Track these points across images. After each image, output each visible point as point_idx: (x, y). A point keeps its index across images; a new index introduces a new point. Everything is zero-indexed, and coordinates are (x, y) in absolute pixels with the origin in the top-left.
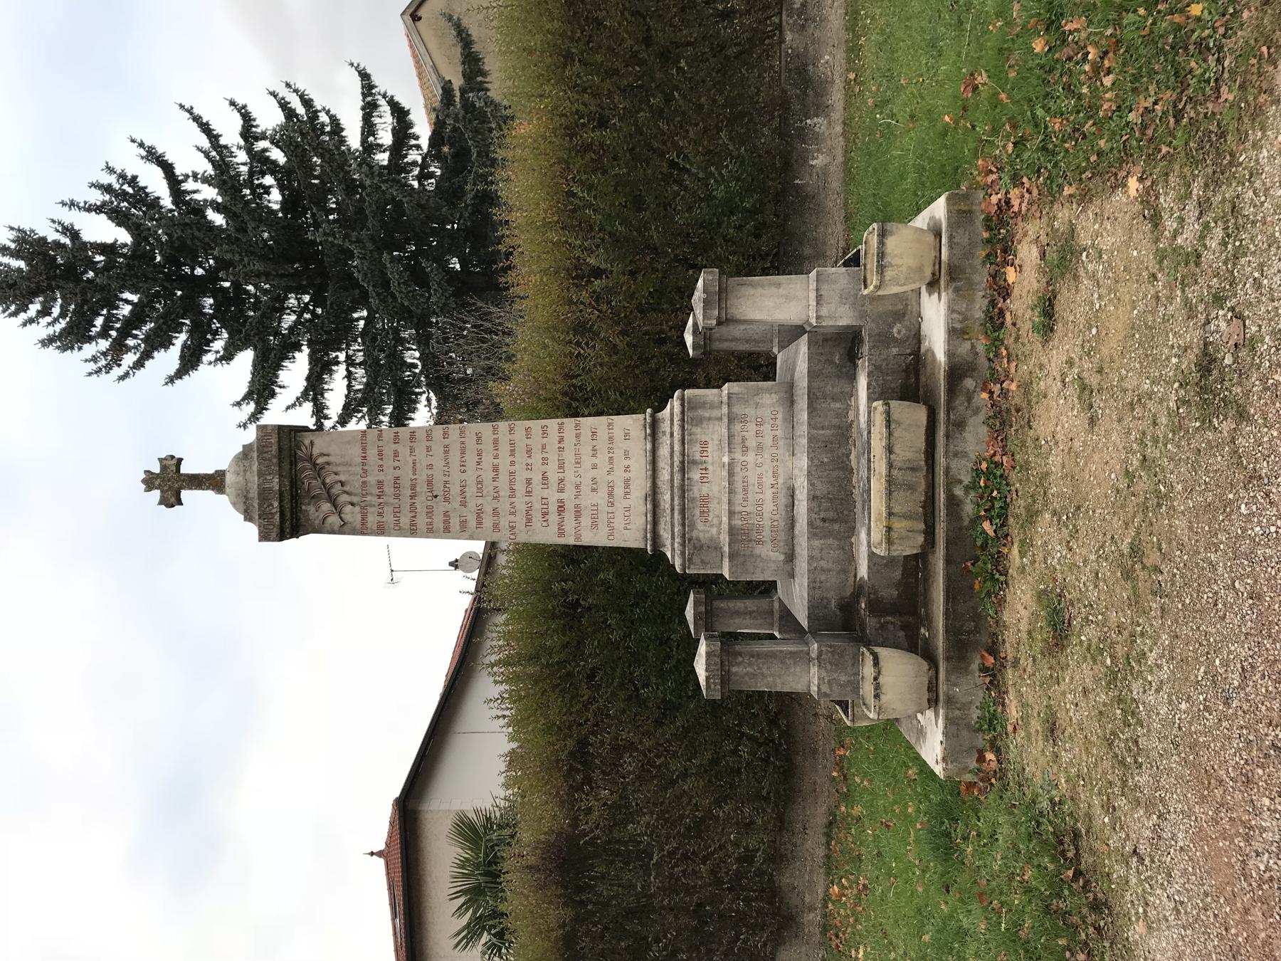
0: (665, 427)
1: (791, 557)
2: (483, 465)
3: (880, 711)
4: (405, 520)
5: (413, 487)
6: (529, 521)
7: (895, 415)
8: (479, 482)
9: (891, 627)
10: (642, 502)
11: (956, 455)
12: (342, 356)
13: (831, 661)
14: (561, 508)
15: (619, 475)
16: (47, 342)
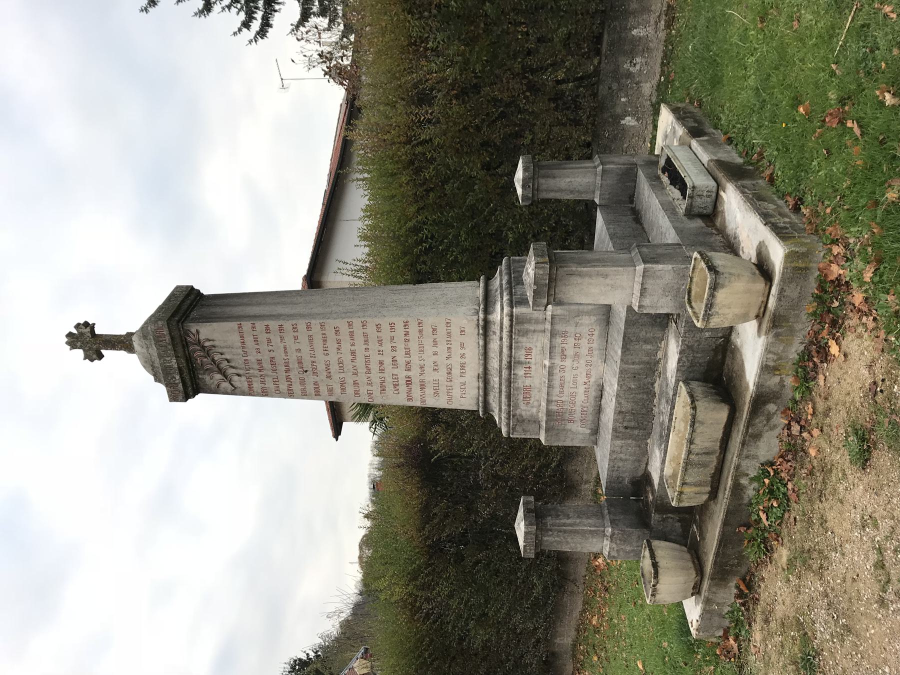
2: (342, 350)
5: (287, 365)
6: (383, 390)
7: (700, 416)
10: (475, 379)
11: (747, 457)
14: (409, 382)
15: (456, 361)
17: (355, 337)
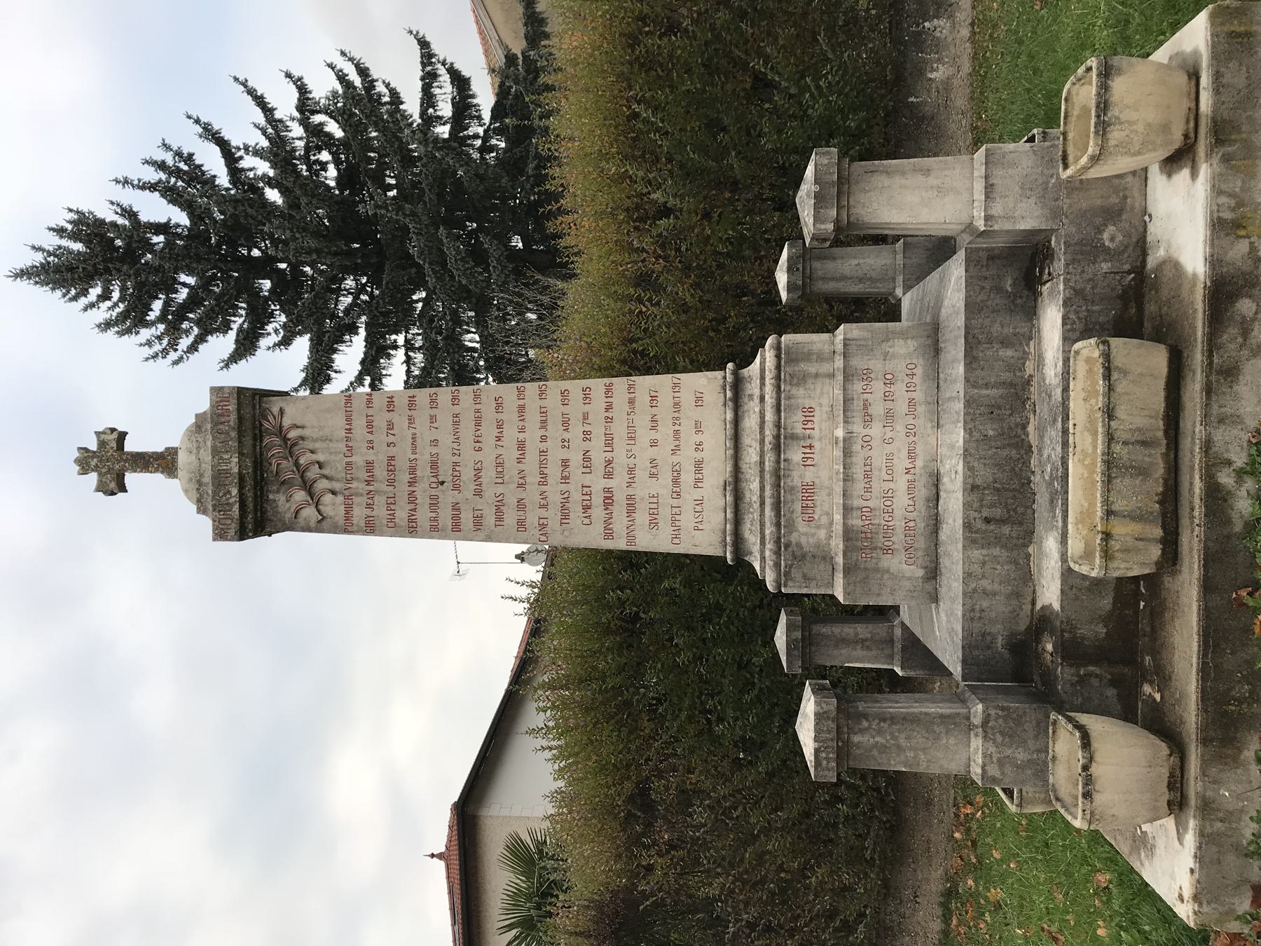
0: (753, 388)
1: (933, 573)
3: (1091, 817)
4: (402, 515)
5: (413, 470)
6: (565, 516)
7: (1119, 359)
8: (499, 465)
9: (1095, 682)
10: (719, 492)
11: (1221, 421)
12: (401, 339)
13: (1000, 731)
14: (608, 501)
15: (687, 456)
16: (107, 325)
17: (527, 415)
